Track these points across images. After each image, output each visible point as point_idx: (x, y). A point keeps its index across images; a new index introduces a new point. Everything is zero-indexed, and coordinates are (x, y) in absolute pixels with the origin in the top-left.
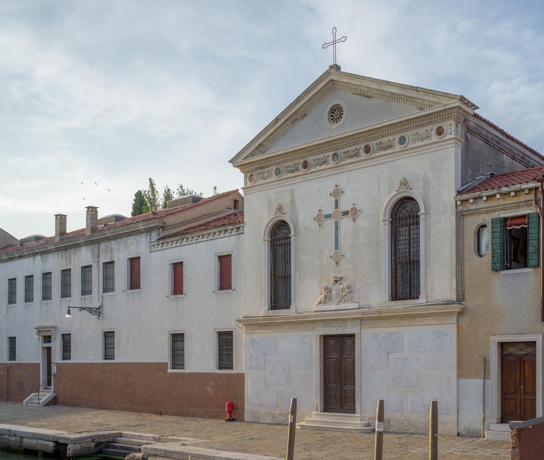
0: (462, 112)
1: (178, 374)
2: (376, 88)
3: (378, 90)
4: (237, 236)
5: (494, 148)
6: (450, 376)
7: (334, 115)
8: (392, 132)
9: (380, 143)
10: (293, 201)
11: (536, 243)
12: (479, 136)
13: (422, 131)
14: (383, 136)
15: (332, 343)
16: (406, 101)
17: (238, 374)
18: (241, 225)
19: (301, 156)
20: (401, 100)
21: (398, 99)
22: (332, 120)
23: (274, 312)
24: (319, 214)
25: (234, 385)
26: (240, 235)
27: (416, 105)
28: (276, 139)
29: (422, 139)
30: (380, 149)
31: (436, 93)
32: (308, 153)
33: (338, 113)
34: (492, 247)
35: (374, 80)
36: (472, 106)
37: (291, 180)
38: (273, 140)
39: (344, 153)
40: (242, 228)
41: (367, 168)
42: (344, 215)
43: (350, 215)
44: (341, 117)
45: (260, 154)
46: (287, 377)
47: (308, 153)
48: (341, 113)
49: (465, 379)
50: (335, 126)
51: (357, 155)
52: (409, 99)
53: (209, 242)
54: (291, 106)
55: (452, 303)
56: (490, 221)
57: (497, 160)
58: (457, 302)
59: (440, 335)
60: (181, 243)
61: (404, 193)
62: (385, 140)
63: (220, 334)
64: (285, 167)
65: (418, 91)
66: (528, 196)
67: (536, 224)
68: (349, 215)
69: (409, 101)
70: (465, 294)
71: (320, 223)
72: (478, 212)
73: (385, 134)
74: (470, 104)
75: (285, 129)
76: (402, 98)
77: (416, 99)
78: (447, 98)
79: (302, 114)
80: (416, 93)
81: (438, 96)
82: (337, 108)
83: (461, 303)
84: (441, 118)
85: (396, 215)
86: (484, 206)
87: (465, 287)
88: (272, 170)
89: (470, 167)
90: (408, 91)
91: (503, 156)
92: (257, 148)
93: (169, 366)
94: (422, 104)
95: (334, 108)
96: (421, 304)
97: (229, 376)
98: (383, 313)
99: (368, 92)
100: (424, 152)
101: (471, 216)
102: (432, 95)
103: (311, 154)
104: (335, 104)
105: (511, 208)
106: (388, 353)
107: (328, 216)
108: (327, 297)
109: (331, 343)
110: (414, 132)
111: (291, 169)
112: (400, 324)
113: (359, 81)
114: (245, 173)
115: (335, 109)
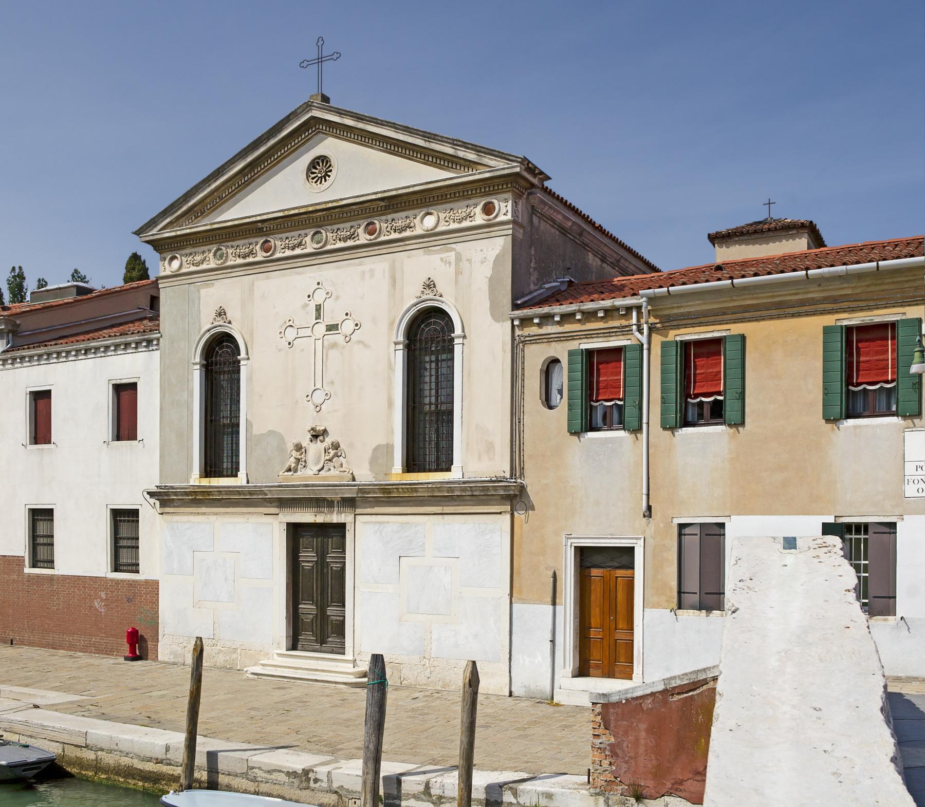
7: (317, 171)
17: (147, 582)
44: (329, 176)
49: (540, 307)
72: (548, 339)
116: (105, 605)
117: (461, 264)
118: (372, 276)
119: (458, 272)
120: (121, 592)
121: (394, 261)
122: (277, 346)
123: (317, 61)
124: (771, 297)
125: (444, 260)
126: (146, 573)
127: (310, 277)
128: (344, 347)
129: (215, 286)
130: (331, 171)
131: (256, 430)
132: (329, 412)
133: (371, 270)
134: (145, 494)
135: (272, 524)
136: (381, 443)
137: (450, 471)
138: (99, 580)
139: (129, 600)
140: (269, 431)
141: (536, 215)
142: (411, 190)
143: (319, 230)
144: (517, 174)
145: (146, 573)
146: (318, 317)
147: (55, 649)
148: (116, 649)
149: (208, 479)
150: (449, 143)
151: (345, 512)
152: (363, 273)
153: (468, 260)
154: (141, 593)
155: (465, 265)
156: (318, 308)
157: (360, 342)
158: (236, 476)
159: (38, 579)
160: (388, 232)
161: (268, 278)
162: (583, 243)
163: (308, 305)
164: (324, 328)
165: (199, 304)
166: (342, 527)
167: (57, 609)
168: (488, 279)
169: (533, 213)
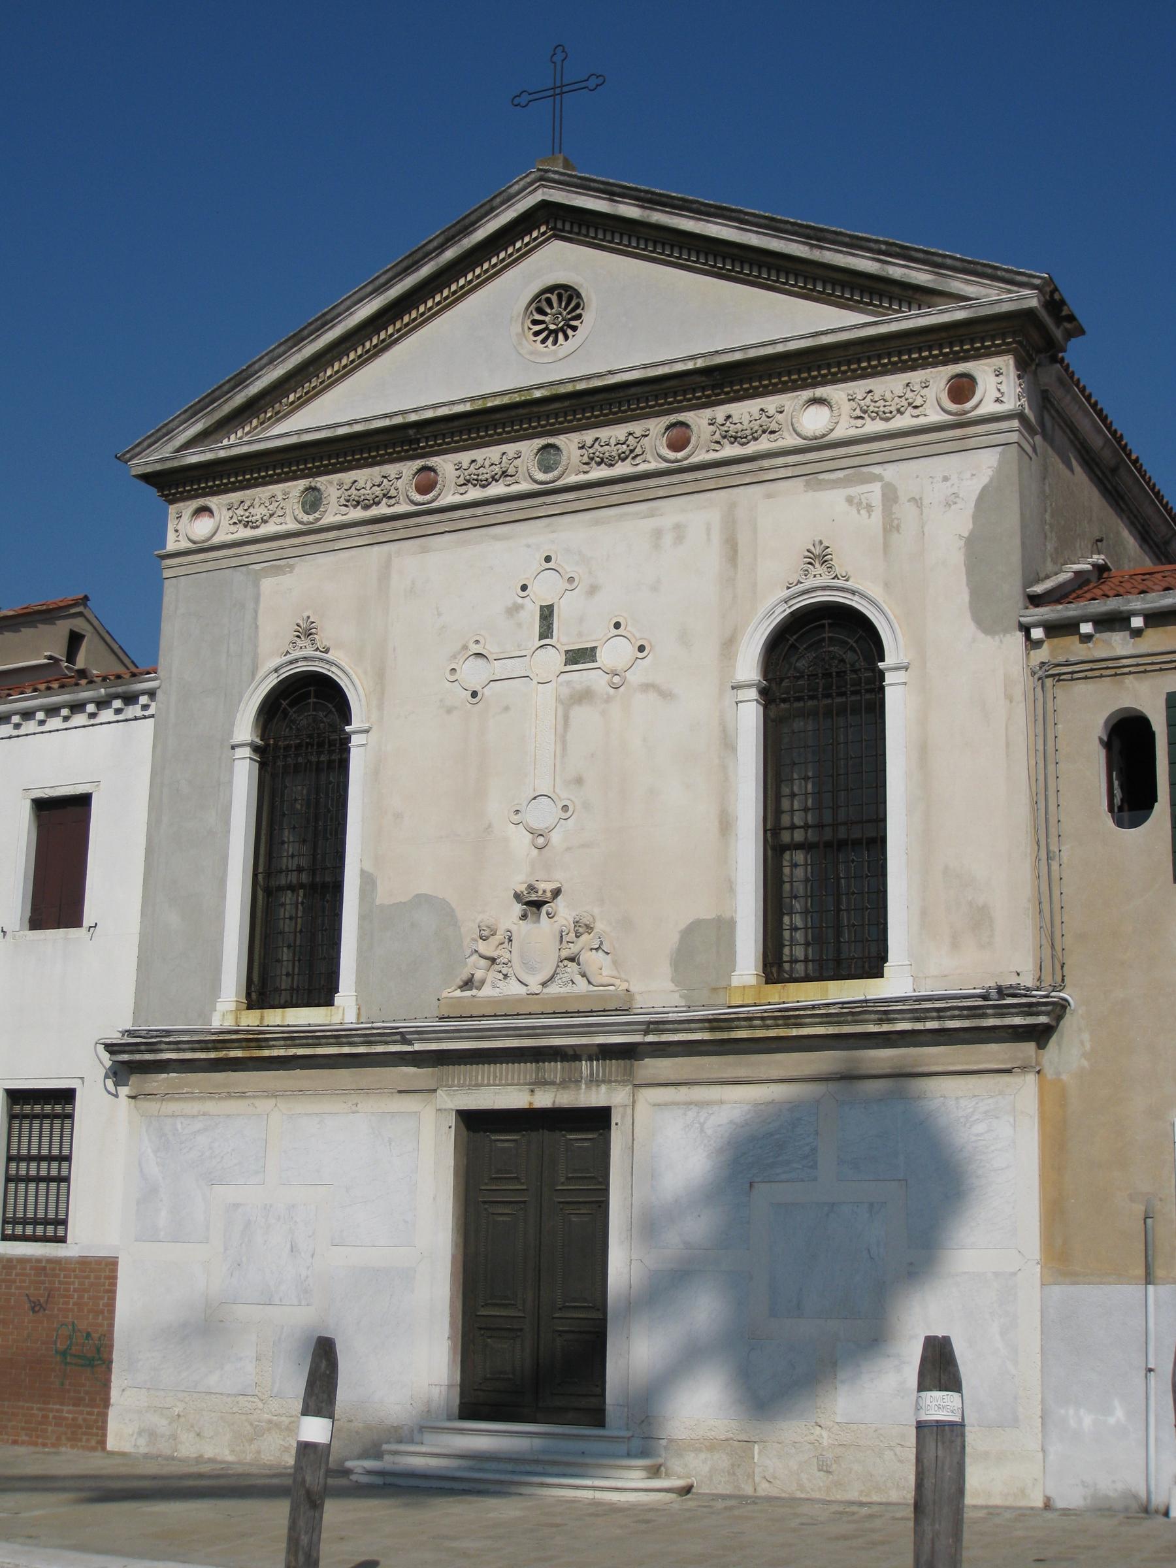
7: (547, 319)
15: (506, 1145)
17: (85, 1263)
23: (262, 1018)
25: (67, 1303)
30: (1002, 374)
46: (307, 1277)
72: (1111, 668)
97: (42, 1267)
106: (751, 1184)
109: (500, 1145)
115: (549, 302)
117: (895, 508)
118: (679, 539)
119: (890, 527)
120: (18, 1288)
121: (733, 506)
122: (441, 701)
124: (860, 1007)
125: (856, 501)
127: (528, 546)
128: (608, 700)
129: (296, 570)
130: (579, 317)
131: (382, 897)
132: (568, 849)
133: (678, 527)
134: (101, 1048)
135: (417, 1114)
136: (703, 916)
137: (882, 976)
139: (36, 1307)
140: (418, 896)
141: (1048, 411)
142: (780, 348)
143: (551, 440)
144: (1029, 313)
146: (546, 630)
149: (257, 1012)
150: (869, 250)
151: (610, 1082)
152: (658, 534)
153: (913, 499)
154: (67, 1290)
155: (906, 512)
156: (547, 614)
157: (647, 687)
160: (718, 442)
161: (424, 550)
162: (1117, 491)
163: (522, 607)
164: (562, 658)
165: (256, 612)
166: (599, 1119)
168: (962, 543)
169: (1044, 407)
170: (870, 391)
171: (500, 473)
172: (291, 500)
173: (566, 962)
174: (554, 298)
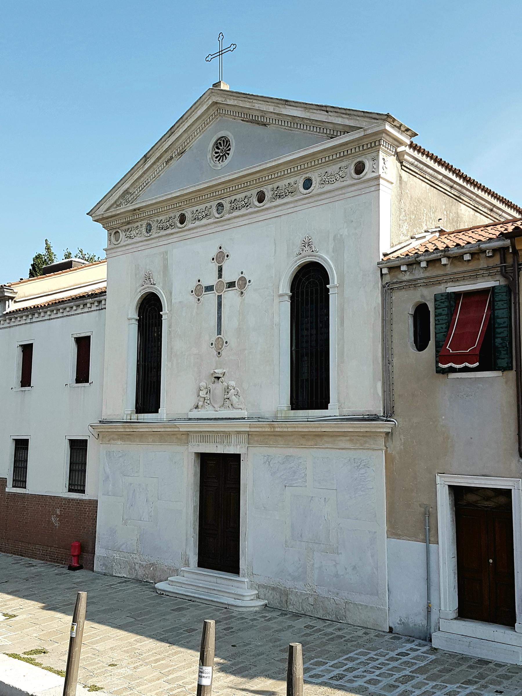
0: (391, 140)
1: (18, 495)
2: (272, 111)
3: (275, 113)
4: (98, 311)
5: (445, 195)
6: (375, 532)
7: (219, 151)
8: (293, 172)
9: (278, 187)
10: (166, 268)
11: (505, 334)
12: (421, 176)
13: (333, 169)
14: (281, 178)
16: (312, 128)
18: (102, 298)
19: (177, 207)
20: (305, 126)
21: (302, 126)
22: (217, 157)
24: (198, 285)
26: (101, 311)
27: (322, 132)
28: (146, 184)
29: (333, 181)
31: (352, 112)
32: (185, 203)
33: (225, 148)
34: (436, 337)
35: (268, 100)
36: (407, 131)
37: (164, 238)
38: (143, 187)
39: (231, 203)
40: (103, 302)
41: (260, 223)
42: (229, 287)
43: (237, 287)
44: (228, 154)
45: (126, 205)
47: (185, 203)
48: (228, 148)
49: (398, 539)
50: (220, 165)
51: (248, 206)
52: (316, 123)
53: (65, 318)
54: (163, 140)
55: (374, 418)
56: (433, 297)
57: (450, 212)
58: (384, 417)
59: (359, 465)
60: (31, 319)
61: (307, 258)
62: (283, 183)
63: (73, 443)
64: (157, 221)
65: (327, 112)
66: (491, 260)
67: (505, 303)
68: (235, 287)
69: (317, 127)
70: (395, 406)
71: (199, 297)
73: (284, 174)
74: (403, 129)
75: (158, 170)
76: (307, 123)
77: (325, 124)
78: (368, 120)
79: (179, 151)
80: (326, 115)
81: (355, 117)
82: (224, 141)
83: (389, 419)
84: (361, 149)
85: (298, 289)
86: (422, 275)
87: (395, 396)
88: (141, 225)
89: (406, 220)
90: (314, 113)
91: (460, 206)
92: (123, 196)
93: (10, 483)
94: (334, 131)
95: (219, 141)
96: (330, 416)
98: (277, 427)
99: (262, 118)
100: (336, 198)
101: (403, 290)
102: (347, 116)
103: (189, 204)
104: (220, 136)
105: (464, 278)
107: (210, 288)
108: (205, 400)
110: (323, 171)
111: (164, 224)
112: (302, 445)
113: (250, 102)
114: (109, 229)
115: (220, 143)
116: (58, 520)
120: (71, 509)
123: (218, 54)
126: (89, 494)
138: (56, 499)
145: (89, 494)
147: (22, 556)
148: (64, 559)
158: (157, 412)
159: (14, 497)
167: (26, 523)
170: (327, 172)
171: (205, 215)
172: (143, 228)
173: (226, 400)
174: (222, 142)
